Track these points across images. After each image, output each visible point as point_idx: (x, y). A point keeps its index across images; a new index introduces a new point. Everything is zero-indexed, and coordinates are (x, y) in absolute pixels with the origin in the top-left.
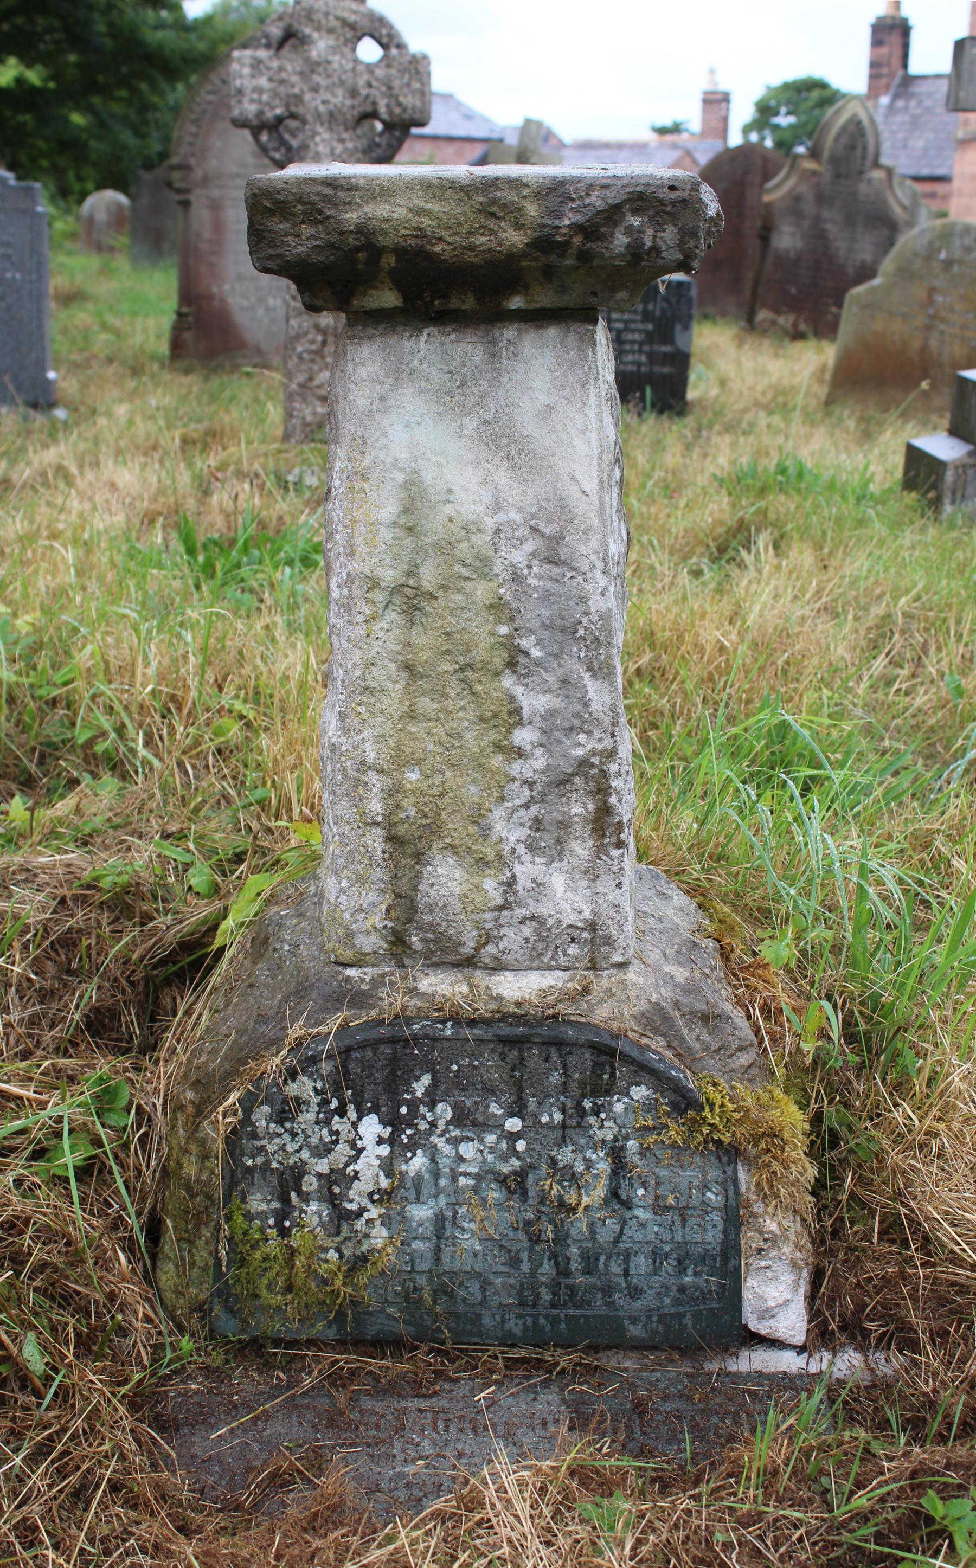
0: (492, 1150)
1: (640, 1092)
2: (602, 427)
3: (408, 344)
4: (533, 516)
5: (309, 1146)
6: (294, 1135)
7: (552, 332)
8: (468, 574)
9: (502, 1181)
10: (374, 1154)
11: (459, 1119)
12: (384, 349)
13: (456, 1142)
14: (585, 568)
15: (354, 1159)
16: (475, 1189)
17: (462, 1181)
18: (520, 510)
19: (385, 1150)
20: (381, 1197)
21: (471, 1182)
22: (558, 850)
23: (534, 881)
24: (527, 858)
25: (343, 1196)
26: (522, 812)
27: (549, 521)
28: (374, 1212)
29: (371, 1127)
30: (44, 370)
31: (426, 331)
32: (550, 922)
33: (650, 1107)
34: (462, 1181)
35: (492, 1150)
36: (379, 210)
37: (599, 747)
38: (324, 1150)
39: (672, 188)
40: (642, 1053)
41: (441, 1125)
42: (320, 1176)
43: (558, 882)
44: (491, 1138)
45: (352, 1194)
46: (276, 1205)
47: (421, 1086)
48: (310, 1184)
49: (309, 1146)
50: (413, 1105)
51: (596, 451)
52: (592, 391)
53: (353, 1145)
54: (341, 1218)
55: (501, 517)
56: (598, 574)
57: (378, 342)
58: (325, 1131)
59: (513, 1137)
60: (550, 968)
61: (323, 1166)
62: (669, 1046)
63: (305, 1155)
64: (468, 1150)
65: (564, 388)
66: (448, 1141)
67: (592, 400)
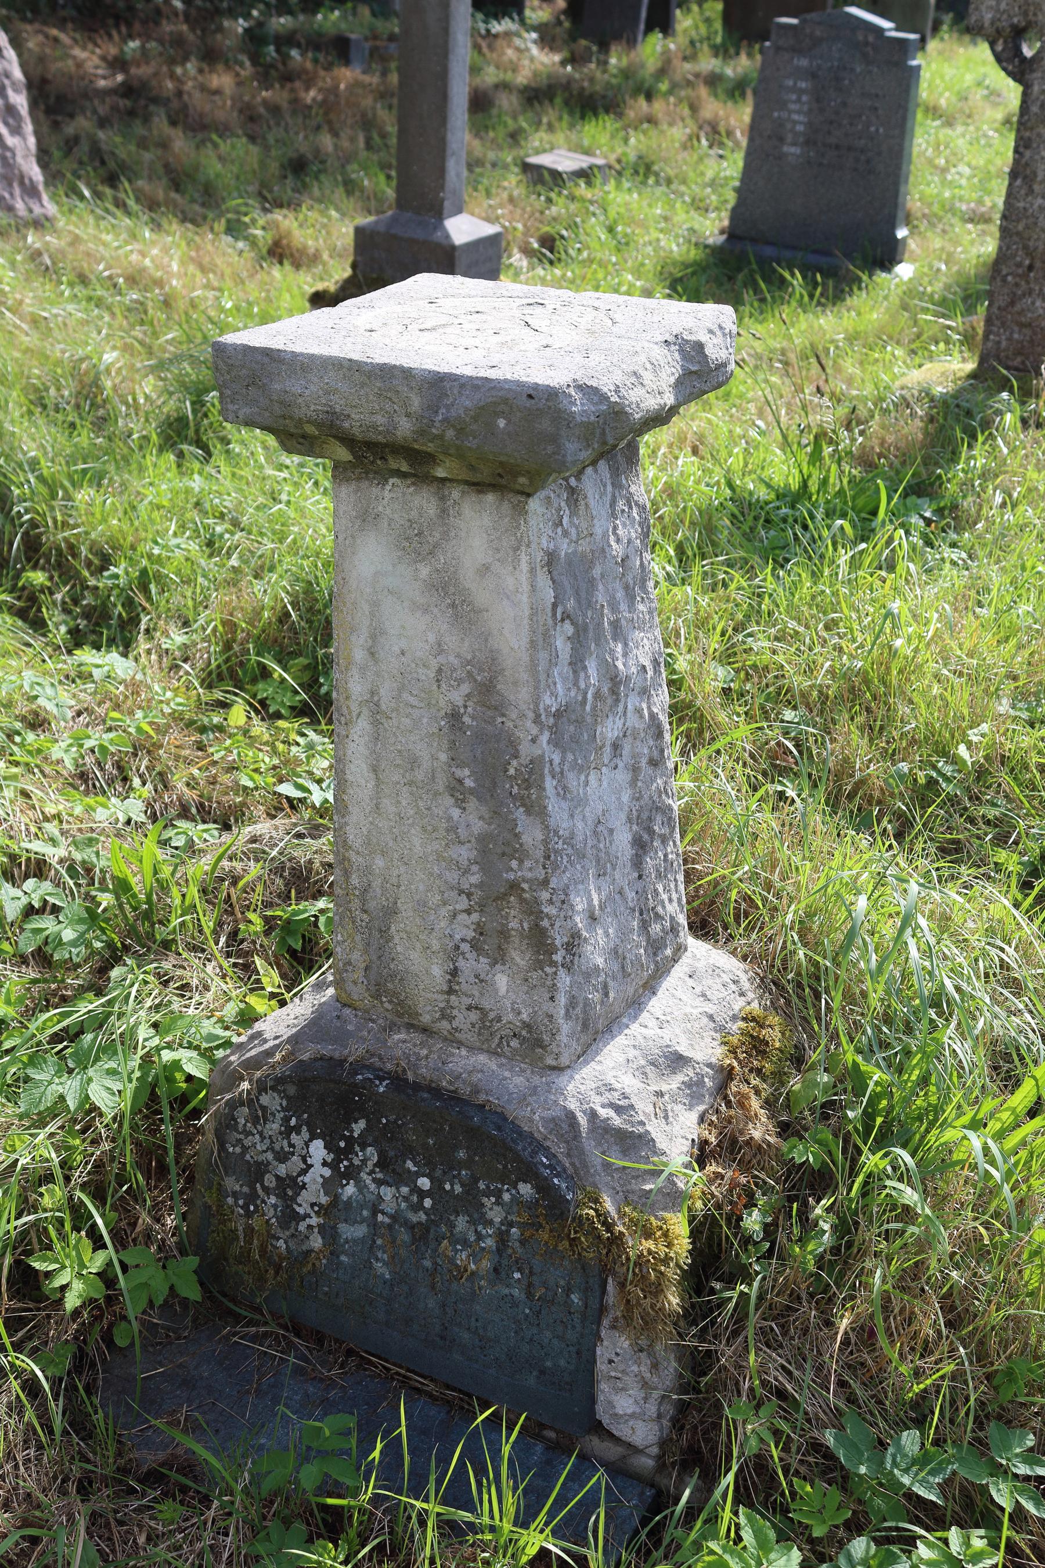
0: (406, 1199)
1: (526, 1189)
2: (533, 588)
3: (375, 491)
4: (469, 663)
5: (272, 1149)
6: (263, 1138)
7: (490, 498)
8: (416, 703)
9: (412, 1227)
10: (318, 1173)
11: (382, 1164)
12: (356, 491)
13: (379, 1183)
14: (514, 716)
15: (304, 1172)
16: (390, 1227)
17: (380, 1217)
18: (458, 656)
19: (327, 1172)
20: (323, 1210)
21: (387, 1220)
22: (499, 958)
23: (477, 976)
24: (472, 956)
25: (293, 1199)
26: (464, 916)
27: (481, 670)
28: (314, 1221)
29: (318, 1150)
30: (893, 228)
31: (391, 481)
32: (492, 1015)
33: (531, 1206)
34: (380, 1217)
35: (406, 1199)
36: (295, 386)
37: (529, 875)
38: (283, 1157)
39: (530, 396)
40: (534, 1153)
41: (370, 1164)
42: (277, 1177)
43: (502, 982)
44: (405, 1190)
45: (299, 1200)
46: (245, 1189)
47: (359, 1127)
48: (269, 1181)
49: (272, 1149)
50: (350, 1140)
51: (527, 613)
52: (524, 559)
53: (305, 1161)
54: (290, 1217)
55: (441, 659)
56: (529, 724)
57: (353, 485)
58: (285, 1143)
59: (422, 1194)
60: (496, 1053)
61: (282, 1170)
62: (569, 1155)
63: (270, 1156)
64: (387, 1193)
65: (498, 550)
66: (374, 1180)
67: (524, 566)
